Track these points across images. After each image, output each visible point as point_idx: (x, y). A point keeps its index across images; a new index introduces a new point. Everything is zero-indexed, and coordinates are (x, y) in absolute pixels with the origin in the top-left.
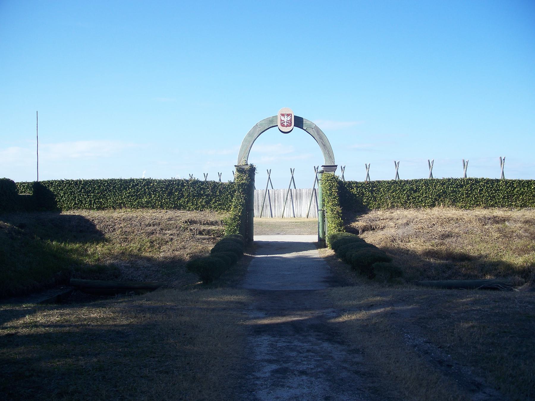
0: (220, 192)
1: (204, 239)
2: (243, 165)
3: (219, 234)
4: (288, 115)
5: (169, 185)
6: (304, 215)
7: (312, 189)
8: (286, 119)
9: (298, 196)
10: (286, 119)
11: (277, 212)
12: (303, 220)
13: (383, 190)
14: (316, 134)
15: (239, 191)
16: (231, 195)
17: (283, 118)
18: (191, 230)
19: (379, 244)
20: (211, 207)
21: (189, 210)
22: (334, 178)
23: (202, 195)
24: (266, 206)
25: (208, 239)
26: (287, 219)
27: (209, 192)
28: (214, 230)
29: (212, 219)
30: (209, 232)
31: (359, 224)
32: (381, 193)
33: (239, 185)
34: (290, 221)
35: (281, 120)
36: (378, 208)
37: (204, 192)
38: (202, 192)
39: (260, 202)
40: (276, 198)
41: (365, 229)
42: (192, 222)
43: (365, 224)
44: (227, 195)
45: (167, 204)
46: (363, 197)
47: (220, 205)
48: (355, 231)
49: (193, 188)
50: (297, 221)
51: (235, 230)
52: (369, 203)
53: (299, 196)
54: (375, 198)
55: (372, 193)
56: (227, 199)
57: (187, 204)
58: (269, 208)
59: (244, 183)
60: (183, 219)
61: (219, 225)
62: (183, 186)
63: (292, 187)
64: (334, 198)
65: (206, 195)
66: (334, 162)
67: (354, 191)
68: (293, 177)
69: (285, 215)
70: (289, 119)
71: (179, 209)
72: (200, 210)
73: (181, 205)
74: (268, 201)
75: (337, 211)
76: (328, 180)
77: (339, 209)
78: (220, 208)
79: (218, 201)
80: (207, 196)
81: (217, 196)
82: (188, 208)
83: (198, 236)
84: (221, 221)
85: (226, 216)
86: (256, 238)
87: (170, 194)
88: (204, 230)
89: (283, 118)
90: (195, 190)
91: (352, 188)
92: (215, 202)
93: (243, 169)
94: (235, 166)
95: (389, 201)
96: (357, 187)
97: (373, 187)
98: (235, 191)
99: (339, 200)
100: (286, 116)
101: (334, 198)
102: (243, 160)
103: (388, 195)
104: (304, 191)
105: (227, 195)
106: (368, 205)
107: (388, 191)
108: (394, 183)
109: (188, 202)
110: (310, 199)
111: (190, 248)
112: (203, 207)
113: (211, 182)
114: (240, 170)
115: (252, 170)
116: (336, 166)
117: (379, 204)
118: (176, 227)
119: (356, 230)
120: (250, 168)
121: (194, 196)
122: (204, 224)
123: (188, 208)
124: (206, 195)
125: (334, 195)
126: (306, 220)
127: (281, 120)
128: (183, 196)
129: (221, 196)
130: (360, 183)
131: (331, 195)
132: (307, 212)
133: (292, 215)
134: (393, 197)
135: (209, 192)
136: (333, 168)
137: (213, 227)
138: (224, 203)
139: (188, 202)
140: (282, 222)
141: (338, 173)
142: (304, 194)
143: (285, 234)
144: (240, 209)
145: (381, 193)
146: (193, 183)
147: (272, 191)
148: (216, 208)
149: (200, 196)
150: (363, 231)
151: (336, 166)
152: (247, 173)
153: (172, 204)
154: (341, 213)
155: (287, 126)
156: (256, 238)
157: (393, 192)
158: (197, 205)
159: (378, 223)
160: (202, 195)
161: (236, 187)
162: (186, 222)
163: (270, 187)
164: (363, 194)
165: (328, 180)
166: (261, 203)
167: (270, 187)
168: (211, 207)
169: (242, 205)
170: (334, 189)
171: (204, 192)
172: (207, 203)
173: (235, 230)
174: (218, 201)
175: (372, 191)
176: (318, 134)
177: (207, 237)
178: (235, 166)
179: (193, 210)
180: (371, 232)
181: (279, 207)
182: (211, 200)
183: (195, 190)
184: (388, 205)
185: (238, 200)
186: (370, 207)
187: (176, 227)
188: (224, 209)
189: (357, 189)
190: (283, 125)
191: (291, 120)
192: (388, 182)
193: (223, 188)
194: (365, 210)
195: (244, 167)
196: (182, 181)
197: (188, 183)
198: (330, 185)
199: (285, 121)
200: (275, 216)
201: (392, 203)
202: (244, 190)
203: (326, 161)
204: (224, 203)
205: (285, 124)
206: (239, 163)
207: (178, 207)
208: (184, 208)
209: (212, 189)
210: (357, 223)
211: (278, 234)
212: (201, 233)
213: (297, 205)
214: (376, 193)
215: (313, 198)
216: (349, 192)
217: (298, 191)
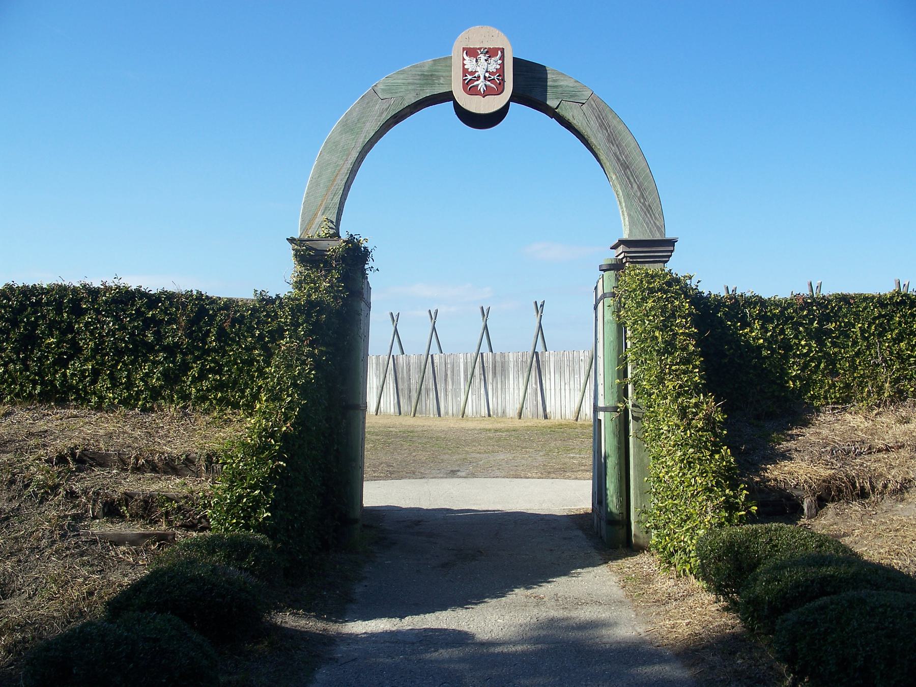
0: (222, 335)
1: (117, 541)
2: (321, 239)
3: (188, 514)
4: (490, 53)
5: (22, 308)
6: (512, 411)
7: (531, 352)
8: (481, 67)
9: (499, 369)
10: (481, 67)
11: (450, 405)
12: (510, 425)
13: (863, 331)
14: (594, 124)
15: (294, 335)
16: (265, 348)
17: (470, 64)
18: (71, 495)
19: (430, 376)
20: (185, 397)
21: (99, 408)
22: (675, 286)
23: (150, 348)
24: (427, 391)
25: (134, 541)
26: (473, 419)
27: (175, 335)
28: (169, 499)
29: (175, 448)
30: (147, 508)
31: (798, 467)
32: (855, 343)
33: (296, 310)
34: (482, 426)
35: (465, 72)
36: (845, 401)
37: (159, 336)
38: (150, 337)
39: (413, 381)
40: (449, 373)
41: (828, 494)
42: (85, 459)
43: (826, 473)
44: (249, 349)
45: (14, 382)
46: (786, 357)
47: (220, 386)
48: (781, 505)
49: (117, 319)
50: (498, 426)
51: (257, 504)
52: (808, 384)
53: (501, 369)
54: (832, 361)
55: (821, 344)
56: (250, 362)
57: (94, 382)
58: (432, 395)
59: (319, 303)
60: (61, 445)
61: (198, 474)
62: (78, 312)
63: (485, 348)
64: (686, 361)
65: (165, 349)
66: (661, 229)
67: (754, 334)
68: (486, 327)
69: (469, 410)
70: (494, 66)
71: (62, 402)
72: (144, 410)
73: (68, 388)
74: (431, 381)
75: (708, 419)
76: (652, 291)
77: (709, 405)
78: (220, 401)
79: (211, 370)
80: (171, 350)
81: (208, 352)
82: (94, 399)
83: (100, 527)
84: (209, 458)
85: (224, 433)
86: (376, 494)
87: (29, 341)
88: (128, 497)
89: (470, 64)
90: (123, 328)
91: (746, 324)
92: (202, 376)
93: (321, 253)
94: (292, 240)
95: (883, 374)
96: (765, 319)
97: (825, 318)
98: (278, 333)
99: (708, 369)
100: (483, 57)
101: (686, 361)
102: (320, 218)
103: (883, 349)
104: (511, 358)
105: (249, 349)
106: (806, 388)
107: (881, 335)
108: (903, 302)
109: (96, 373)
110: (526, 375)
111: (29, 590)
112: (156, 394)
113: (188, 295)
114: (309, 255)
115: (355, 257)
116: (671, 243)
117: (848, 386)
118: (12, 482)
119: (789, 497)
120: (347, 250)
121: (120, 353)
122: (137, 469)
123: (94, 399)
124: (165, 349)
125: (684, 349)
126: (518, 423)
127: (465, 72)
128: (76, 350)
129: (225, 353)
130: (777, 304)
131: (670, 347)
132: (518, 406)
133: (484, 412)
134: (899, 356)
135: (175, 335)
136: (660, 251)
137: (171, 485)
138: (235, 382)
139: (96, 373)
140: (462, 430)
141: (677, 265)
142: (511, 365)
143: (473, 475)
144: (290, 407)
145: (855, 343)
146: (115, 301)
147: (440, 358)
148: (203, 399)
149: (140, 350)
150: (821, 502)
151: (671, 243)
152: (338, 272)
153: (35, 383)
154: (725, 424)
155: (488, 92)
156: (376, 494)
157: (898, 340)
158: (129, 385)
159: (873, 464)
160: (150, 348)
161: (284, 317)
162: (62, 459)
163: (434, 349)
164: (787, 346)
165: (652, 291)
166: (414, 386)
167: (434, 349)
168: (185, 397)
169: (304, 390)
170: (680, 326)
171: (159, 336)
172: (172, 378)
173: (257, 504)
174: (211, 370)
175: (819, 336)
176: (602, 125)
177: (137, 529)
178: (292, 240)
179: (112, 408)
180: (856, 506)
181: (456, 394)
182: (185, 368)
183: (123, 328)
184: (880, 389)
185: (289, 367)
186: (813, 397)
187: (12, 482)
188: (236, 406)
189: (764, 329)
190: (471, 89)
191: (501, 71)
192: (881, 302)
193: (234, 321)
194: (794, 411)
195: (323, 245)
196: (75, 290)
197: (95, 301)
198: (664, 309)
199: (481, 72)
200: (447, 413)
201: (897, 380)
202: (315, 328)
203: (632, 223)
204: (235, 382)
205: (481, 84)
206: (305, 230)
207: (56, 396)
208: (82, 399)
209: (192, 322)
210: (787, 466)
211: (453, 474)
212: (112, 511)
213: (495, 390)
214: (834, 344)
215: (534, 373)
216: (734, 340)
217: (498, 358)
